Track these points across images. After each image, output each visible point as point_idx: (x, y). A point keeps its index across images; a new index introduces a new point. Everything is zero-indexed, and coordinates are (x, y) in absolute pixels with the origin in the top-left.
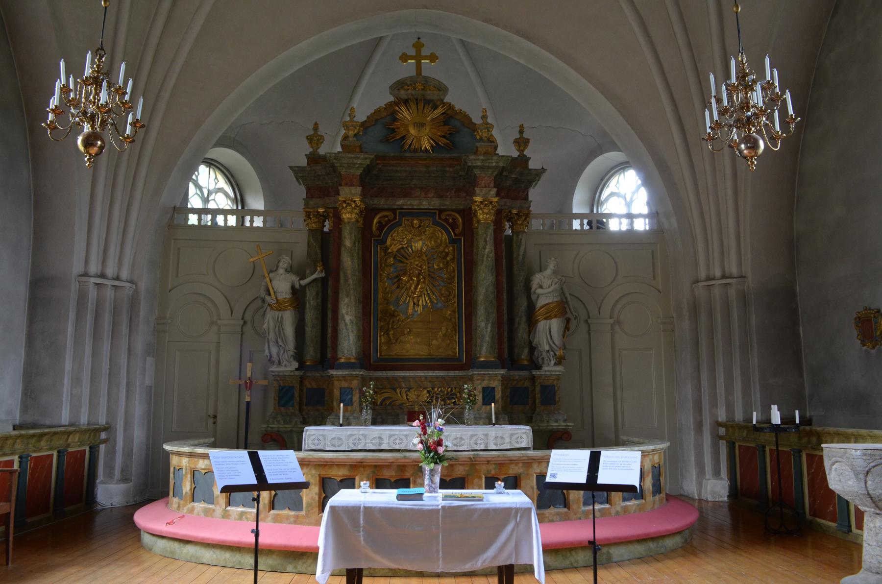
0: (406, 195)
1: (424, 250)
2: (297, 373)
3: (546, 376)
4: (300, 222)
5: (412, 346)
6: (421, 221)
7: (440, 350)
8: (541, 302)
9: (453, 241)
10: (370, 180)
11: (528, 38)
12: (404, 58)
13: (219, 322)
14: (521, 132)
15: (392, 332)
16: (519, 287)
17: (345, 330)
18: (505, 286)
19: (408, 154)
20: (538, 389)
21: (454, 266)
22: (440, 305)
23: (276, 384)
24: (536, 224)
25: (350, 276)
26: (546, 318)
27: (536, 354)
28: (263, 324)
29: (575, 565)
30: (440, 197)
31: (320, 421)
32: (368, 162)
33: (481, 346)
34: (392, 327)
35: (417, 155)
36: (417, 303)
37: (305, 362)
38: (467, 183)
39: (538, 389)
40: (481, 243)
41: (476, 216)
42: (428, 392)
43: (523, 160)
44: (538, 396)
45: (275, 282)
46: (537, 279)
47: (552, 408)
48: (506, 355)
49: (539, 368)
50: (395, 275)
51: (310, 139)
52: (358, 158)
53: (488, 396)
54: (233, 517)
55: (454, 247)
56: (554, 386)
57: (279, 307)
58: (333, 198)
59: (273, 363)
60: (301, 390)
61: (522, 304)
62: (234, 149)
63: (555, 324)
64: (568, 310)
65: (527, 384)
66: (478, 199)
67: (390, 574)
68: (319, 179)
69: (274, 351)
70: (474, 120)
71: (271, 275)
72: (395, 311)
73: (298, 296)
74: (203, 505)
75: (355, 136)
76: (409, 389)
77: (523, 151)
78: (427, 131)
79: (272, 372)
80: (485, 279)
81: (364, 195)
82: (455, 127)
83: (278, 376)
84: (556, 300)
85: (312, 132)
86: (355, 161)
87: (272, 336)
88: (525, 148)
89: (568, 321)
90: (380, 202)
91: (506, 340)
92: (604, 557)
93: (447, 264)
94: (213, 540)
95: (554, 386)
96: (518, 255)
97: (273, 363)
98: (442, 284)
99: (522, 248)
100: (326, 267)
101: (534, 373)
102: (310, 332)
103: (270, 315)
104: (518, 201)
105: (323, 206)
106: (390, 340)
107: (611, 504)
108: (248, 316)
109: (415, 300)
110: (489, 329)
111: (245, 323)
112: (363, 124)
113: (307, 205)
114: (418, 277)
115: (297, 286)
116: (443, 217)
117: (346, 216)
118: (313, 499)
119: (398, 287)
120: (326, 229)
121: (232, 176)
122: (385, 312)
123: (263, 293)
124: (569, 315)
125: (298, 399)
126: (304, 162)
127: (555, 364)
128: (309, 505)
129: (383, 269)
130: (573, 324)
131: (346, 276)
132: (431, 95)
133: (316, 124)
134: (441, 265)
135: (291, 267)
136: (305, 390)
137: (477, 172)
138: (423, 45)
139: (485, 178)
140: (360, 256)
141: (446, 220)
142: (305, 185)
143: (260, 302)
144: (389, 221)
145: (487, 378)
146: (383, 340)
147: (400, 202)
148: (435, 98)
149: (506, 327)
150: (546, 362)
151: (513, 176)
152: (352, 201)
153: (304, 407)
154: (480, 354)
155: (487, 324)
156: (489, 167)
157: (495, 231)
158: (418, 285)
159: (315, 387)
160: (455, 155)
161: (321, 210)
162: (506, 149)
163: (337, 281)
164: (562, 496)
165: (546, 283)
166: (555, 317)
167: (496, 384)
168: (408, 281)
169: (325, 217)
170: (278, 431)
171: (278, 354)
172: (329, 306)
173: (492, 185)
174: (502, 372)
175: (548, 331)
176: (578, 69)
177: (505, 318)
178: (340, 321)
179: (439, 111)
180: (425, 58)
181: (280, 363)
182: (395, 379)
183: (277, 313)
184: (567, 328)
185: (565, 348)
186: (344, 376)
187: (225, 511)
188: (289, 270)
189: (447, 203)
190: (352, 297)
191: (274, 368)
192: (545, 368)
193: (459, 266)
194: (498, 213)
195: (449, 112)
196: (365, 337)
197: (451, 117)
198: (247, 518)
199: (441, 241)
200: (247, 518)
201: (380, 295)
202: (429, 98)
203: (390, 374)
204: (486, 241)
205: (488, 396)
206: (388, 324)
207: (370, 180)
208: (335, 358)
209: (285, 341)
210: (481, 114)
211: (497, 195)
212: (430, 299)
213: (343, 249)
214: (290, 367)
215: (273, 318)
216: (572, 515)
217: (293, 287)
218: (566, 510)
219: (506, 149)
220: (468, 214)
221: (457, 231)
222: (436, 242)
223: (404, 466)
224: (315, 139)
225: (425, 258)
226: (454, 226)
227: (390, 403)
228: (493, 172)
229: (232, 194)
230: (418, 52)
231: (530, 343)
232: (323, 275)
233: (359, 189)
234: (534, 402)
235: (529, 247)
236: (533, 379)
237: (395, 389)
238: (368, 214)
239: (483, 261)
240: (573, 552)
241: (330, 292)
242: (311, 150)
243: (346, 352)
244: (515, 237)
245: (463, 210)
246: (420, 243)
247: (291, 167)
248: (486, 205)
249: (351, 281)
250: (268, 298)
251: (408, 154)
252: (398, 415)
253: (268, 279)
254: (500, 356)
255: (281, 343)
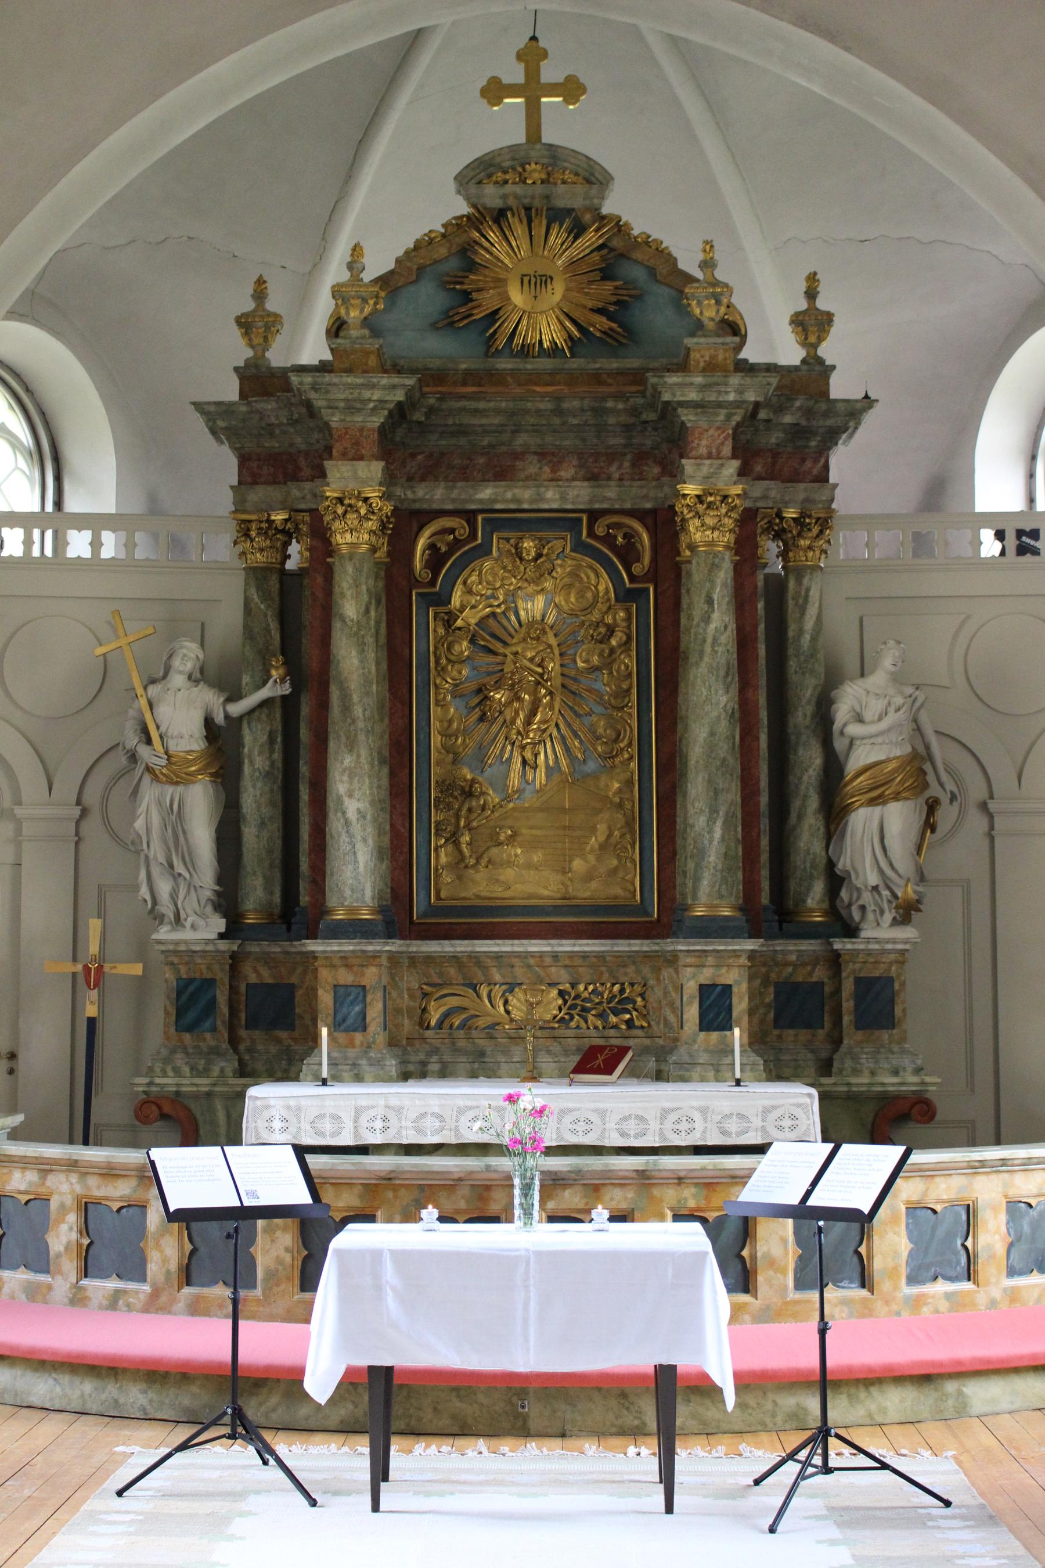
0: (502, 474)
1: (551, 619)
2: (224, 945)
3: (869, 953)
4: (222, 547)
5: (522, 874)
6: (542, 543)
7: (594, 885)
8: (856, 761)
9: (626, 596)
10: (402, 440)
11: (830, 35)
12: (494, 91)
13: (18, 811)
14: (811, 294)
15: (467, 838)
16: (802, 715)
17: (344, 838)
18: (763, 715)
19: (504, 364)
20: (848, 987)
21: (629, 661)
22: (591, 766)
23: (169, 975)
24: (846, 545)
25: (355, 698)
26: (872, 802)
27: (844, 894)
28: (134, 818)
29: (880, 1419)
30: (593, 478)
31: (286, 1069)
32: (400, 396)
33: (697, 880)
34: (468, 827)
35: (530, 365)
36: (530, 764)
37: (242, 916)
38: (663, 441)
39: (848, 987)
40: (699, 608)
41: (684, 529)
42: (561, 993)
43: (816, 372)
44: (848, 1005)
45: (164, 711)
46: (847, 701)
47: (885, 1035)
48: (765, 899)
49: (851, 931)
50: (473, 686)
51: (245, 323)
52: (373, 386)
53: (715, 1009)
54: (95, 1302)
55: (628, 611)
56: (891, 980)
57: (174, 774)
58: (307, 486)
59: (160, 919)
60: (233, 989)
61: (809, 761)
62: (36, 322)
63: (899, 818)
64: (931, 778)
65: (820, 974)
66: (691, 489)
67: (455, 1429)
68: (273, 433)
69: (164, 888)
70: (682, 265)
71: (153, 690)
72: (473, 781)
73: (220, 737)
74: (22, 1275)
75: (366, 322)
76: (511, 987)
77: (815, 346)
78: (558, 297)
79: (159, 942)
80: (710, 702)
81: (390, 479)
82: (633, 293)
83: (175, 952)
84: (897, 752)
85: (249, 306)
86: (367, 394)
87: (157, 851)
88: (820, 340)
89: (932, 806)
90: (435, 494)
91: (765, 857)
92: (950, 1402)
93: (609, 660)
94: (55, 1353)
95: (891, 980)
96: (801, 631)
97: (160, 919)
98: (598, 709)
99: (812, 611)
100: (294, 671)
101: (838, 945)
102: (253, 839)
103: (150, 792)
104: (802, 486)
105: (284, 506)
106: (462, 858)
107: (976, 1283)
108: (92, 797)
109: (528, 755)
110: (718, 833)
111: (84, 813)
112: (383, 280)
113: (240, 505)
114: (534, 693)
115: (219, 719)
116: (600, 531)
117: (343, 539)
118: (279, 1261)
119: (482, 719)
120: (290, 565)
121: (27, 390)
122: (447, 787)
123: (132, 739)
124: (934, 790)
125: (225, 1010)
126: (230, 391)
127: (895, 922)
128: (270, 1275)
129: (442, 671)
130: (946, 816)
131: (345, 697)
132: (568, 196)
133: (260, 282)
134: (595, 660)
135: (202, 670)
136: (243, 988)
137: (687, 417)
138: (545, 54)
139: (709, 434)
140: (383, 639)
141: (608, 540)
142: (233, 448)
143: (124, 760)
144: (457, 543)
145: (710, 960)
146: (443, 859)
147: (486, 493)
148: (577, 203)
149: (765, 824)
150: (870, 916)
151: (788, 419)
152: (358, 497)
153: (243, 1033)
154: (695, 897)
155: (711, 821)
156: (720, 405)
157: (737, 568)
158: (533, 713)
159: (270, 981)
160: (633, 363)
161: (279, 517)
162: (773, 343)
163: (323, 705)
164: (855, 1259)
165: (874, 707)
166: (896, 797)
167: (734, 976)
168: (509, 703)
169: (287, 535)
170: (178, 1093)
171: (174, 896)
172: (304, 769)
173: (727, 450)
174: (750, 945)
175: (878, 837)
176: (965, 118)
177: (764, 799)
178: (331, 815)
179: (590, 239)
180: (552, 89)
181: (178, 920)
182: (476, 959)
183: (170, 789)
184: (929, 825)
185: (922, 878)
186: (345, 960)
187: (77, 1287)
188: (201, 676)
189: (610, 494)
190: (364, 752)
191: (164, 933)
192: (866, 933)
193: (642, 662)
194: (748, 519)
195: (616, 243)
196: (399, 852)
197: (622, 256)
198: (128, 1305)
199: (596, 596)
200: (128, 1305)
201: (436, 740)
202: (560, 203)
203: (462, 946)
204: (710, 601)
205: (715, 1009)
206: (458, 818)
207: (402, 440)
208: (320, 909)
209: (190, 863)
210: (701, 256)
211: (743, 472)
212: (568, 750)
213: (337, 625)
214: (204, 929)
215: (159, 803)
216: (880, 1307)
217: (208, 722)
218: (864, 1293)
219: (773, 343)
220: (665, 523)
221: (637, 569)
222: (581, 595)
223: (488, 1188)
224: (258, 325)
225: (553, 641)
226: (628, 554)
227: (462, 1026)
228: (728, 417)
229: (25, 436)
230: (532, 74)
231: (831, 865)
232: (286, 689)
233: (376, 468)
234: (838, 1022)
235: (829, 606)
236: (835, 961)
237: (474, 987)
238: (403, 524)
239: (701, 653)
240: (874, 1390)
241: (305, 734)
242: (250, 353)
243: (348, 892)
244: (792, 584)
245: (654, 512)
246: (540, 601)
247: (198, 406)
248: (710, 506)
249: (358, 711)
250: (143, 751)
251: (504, 364)
252: (482, 1054)
253: (143, 702)
254: (748, 906)
255: (179, 868)
